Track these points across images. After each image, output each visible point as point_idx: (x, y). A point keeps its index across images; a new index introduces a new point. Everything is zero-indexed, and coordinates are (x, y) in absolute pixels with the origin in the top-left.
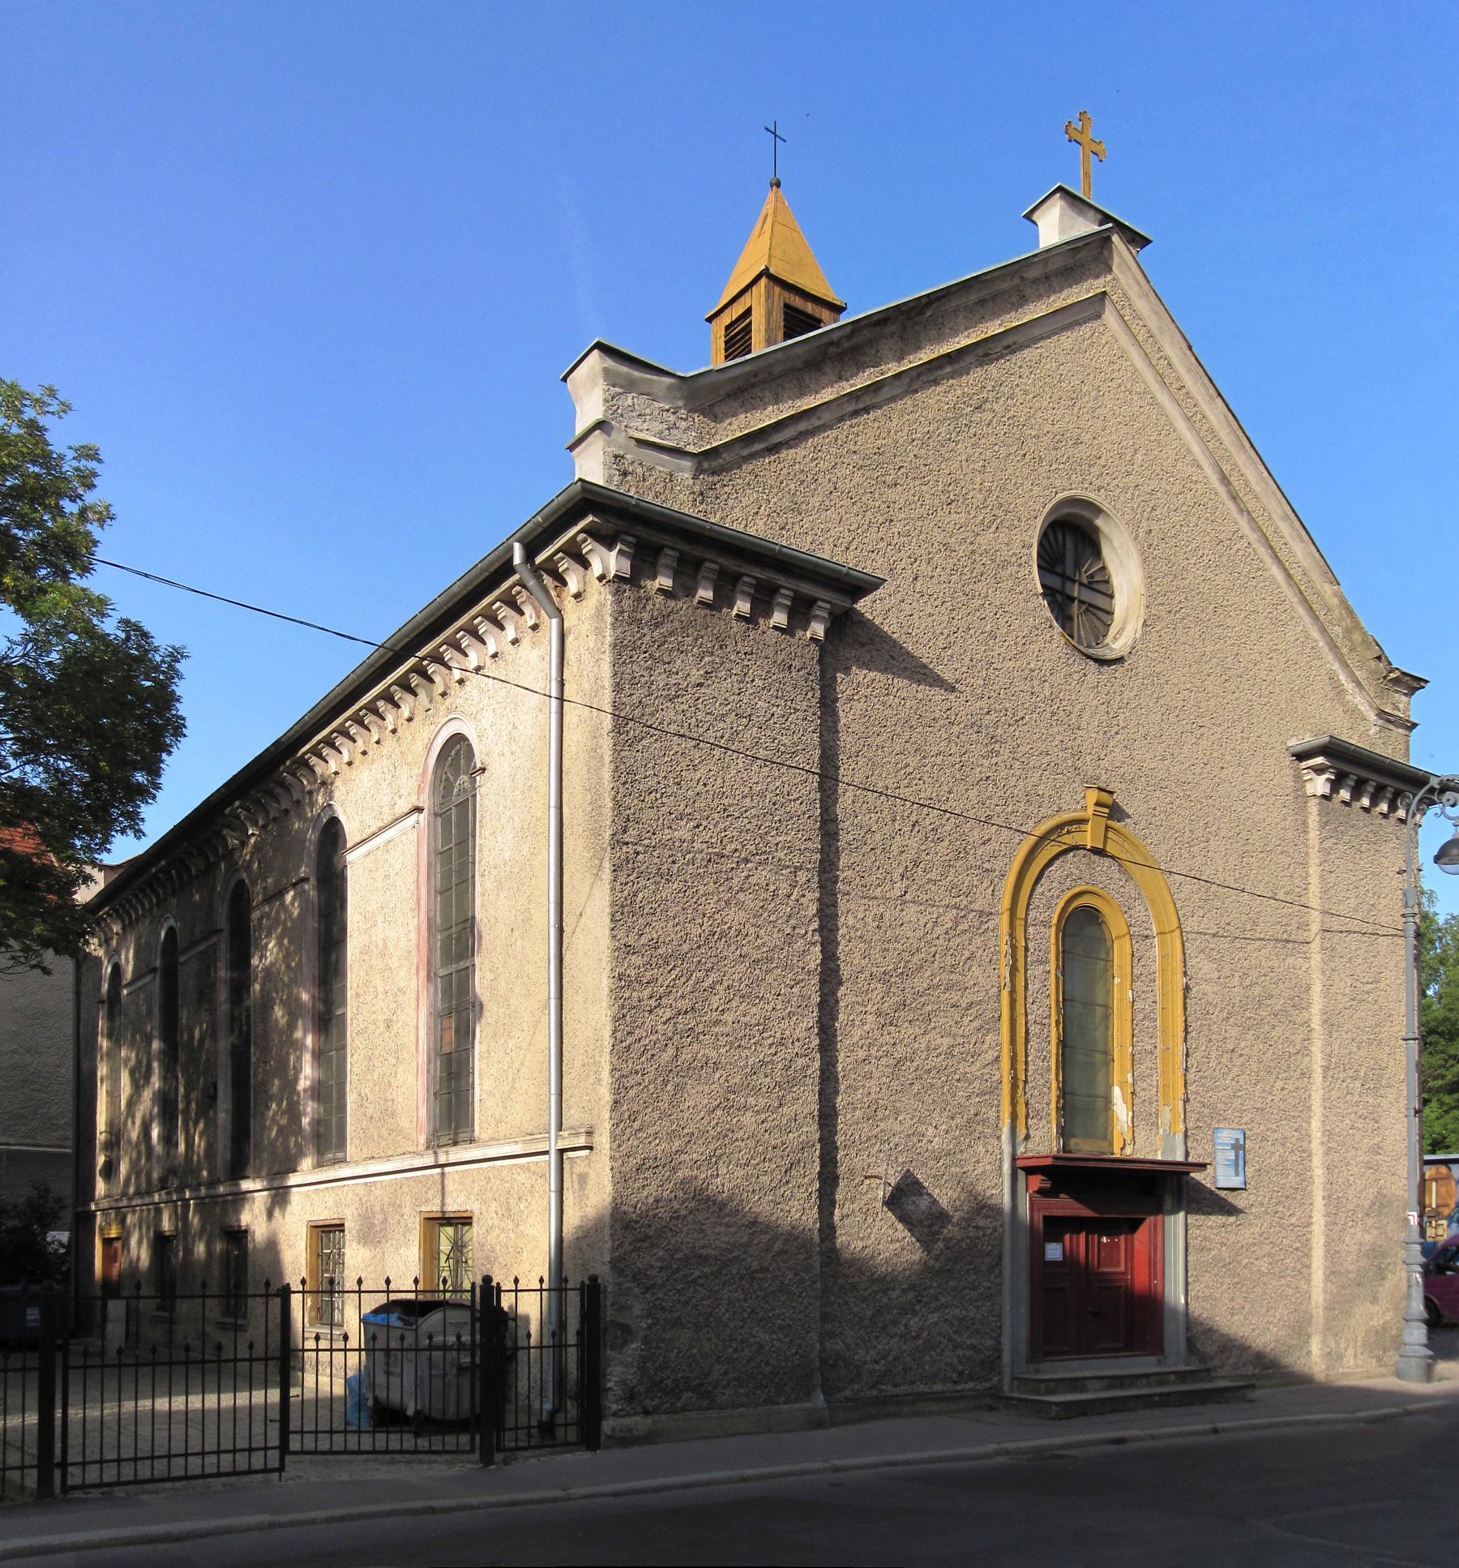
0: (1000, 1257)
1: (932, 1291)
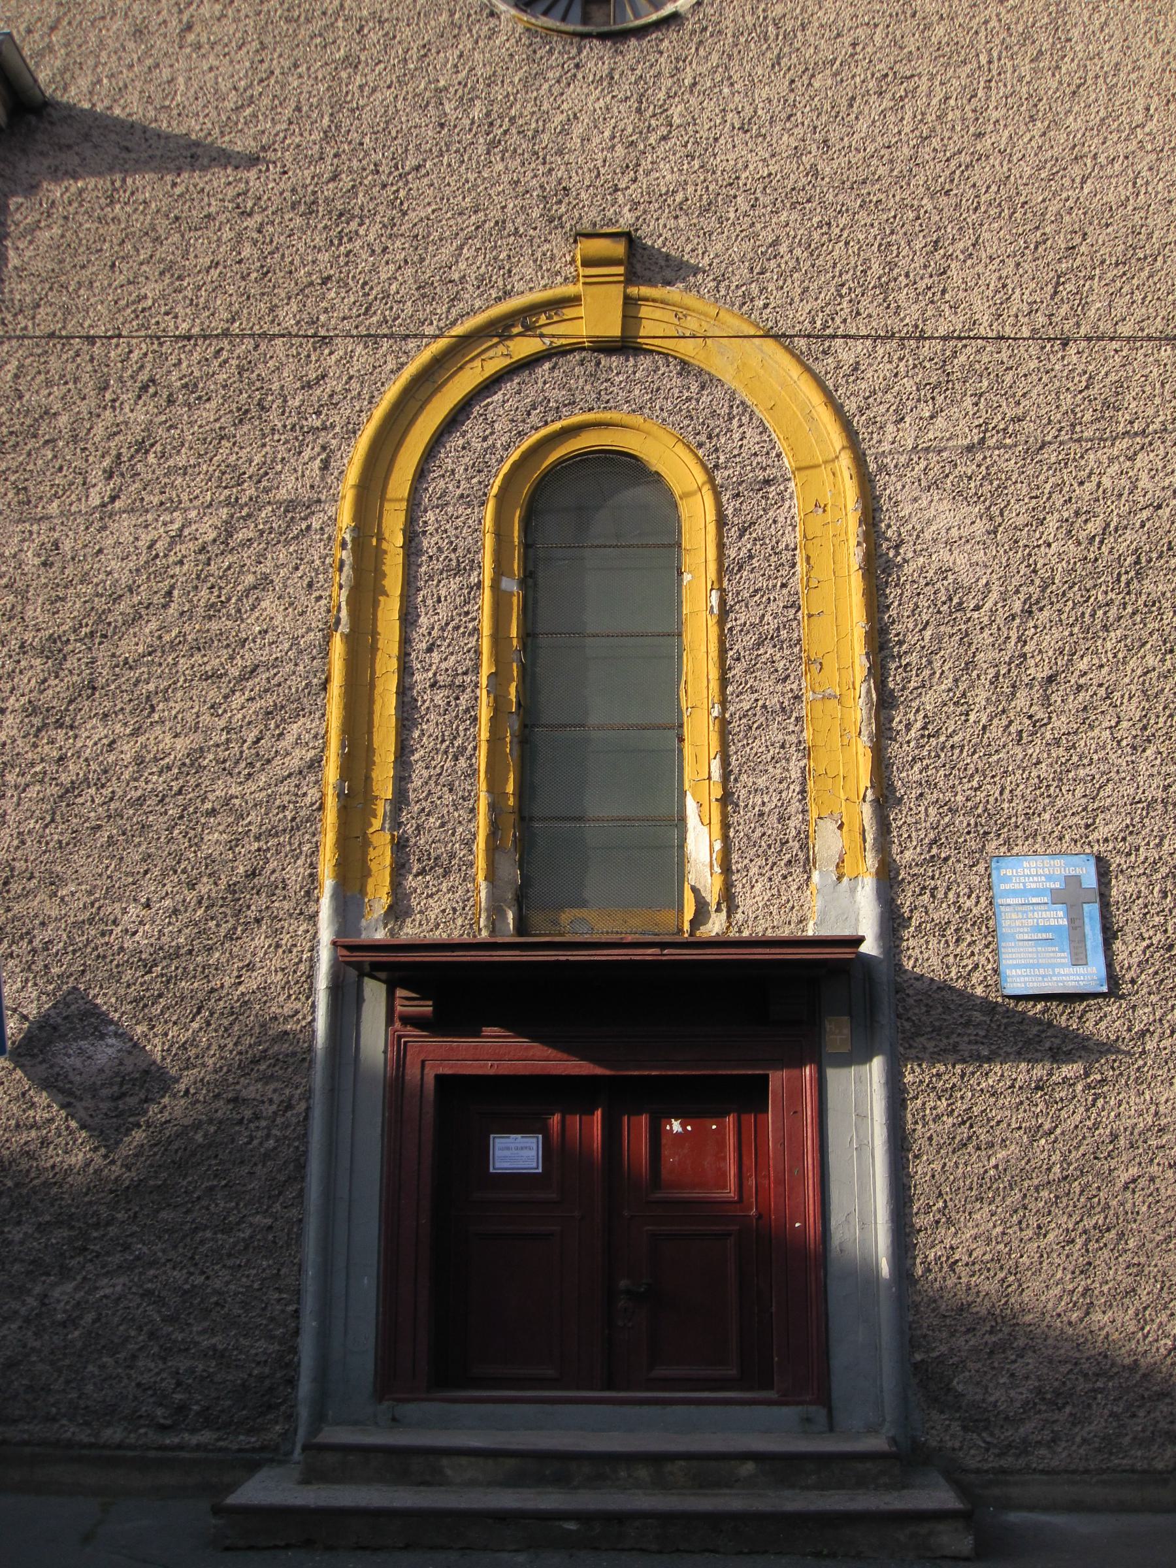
0: (301, 1166)
1: (113, 1231)
